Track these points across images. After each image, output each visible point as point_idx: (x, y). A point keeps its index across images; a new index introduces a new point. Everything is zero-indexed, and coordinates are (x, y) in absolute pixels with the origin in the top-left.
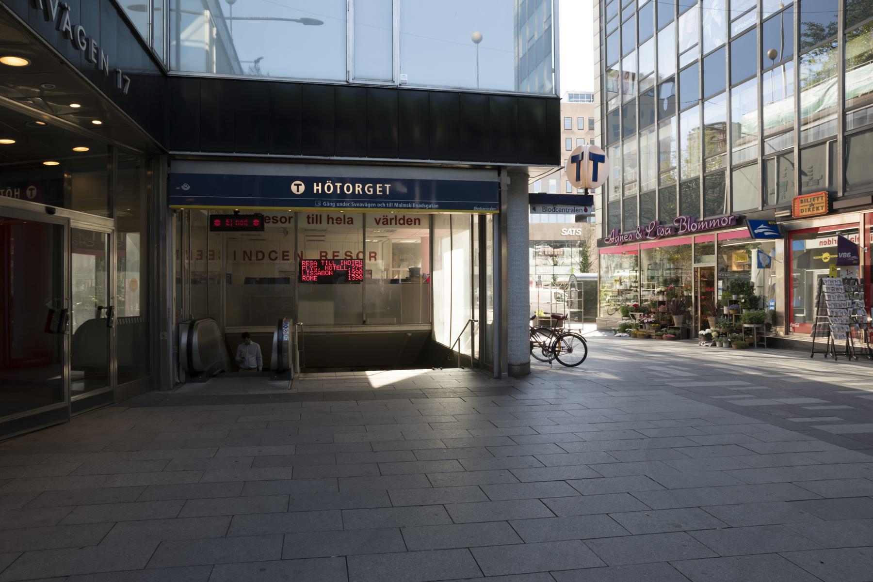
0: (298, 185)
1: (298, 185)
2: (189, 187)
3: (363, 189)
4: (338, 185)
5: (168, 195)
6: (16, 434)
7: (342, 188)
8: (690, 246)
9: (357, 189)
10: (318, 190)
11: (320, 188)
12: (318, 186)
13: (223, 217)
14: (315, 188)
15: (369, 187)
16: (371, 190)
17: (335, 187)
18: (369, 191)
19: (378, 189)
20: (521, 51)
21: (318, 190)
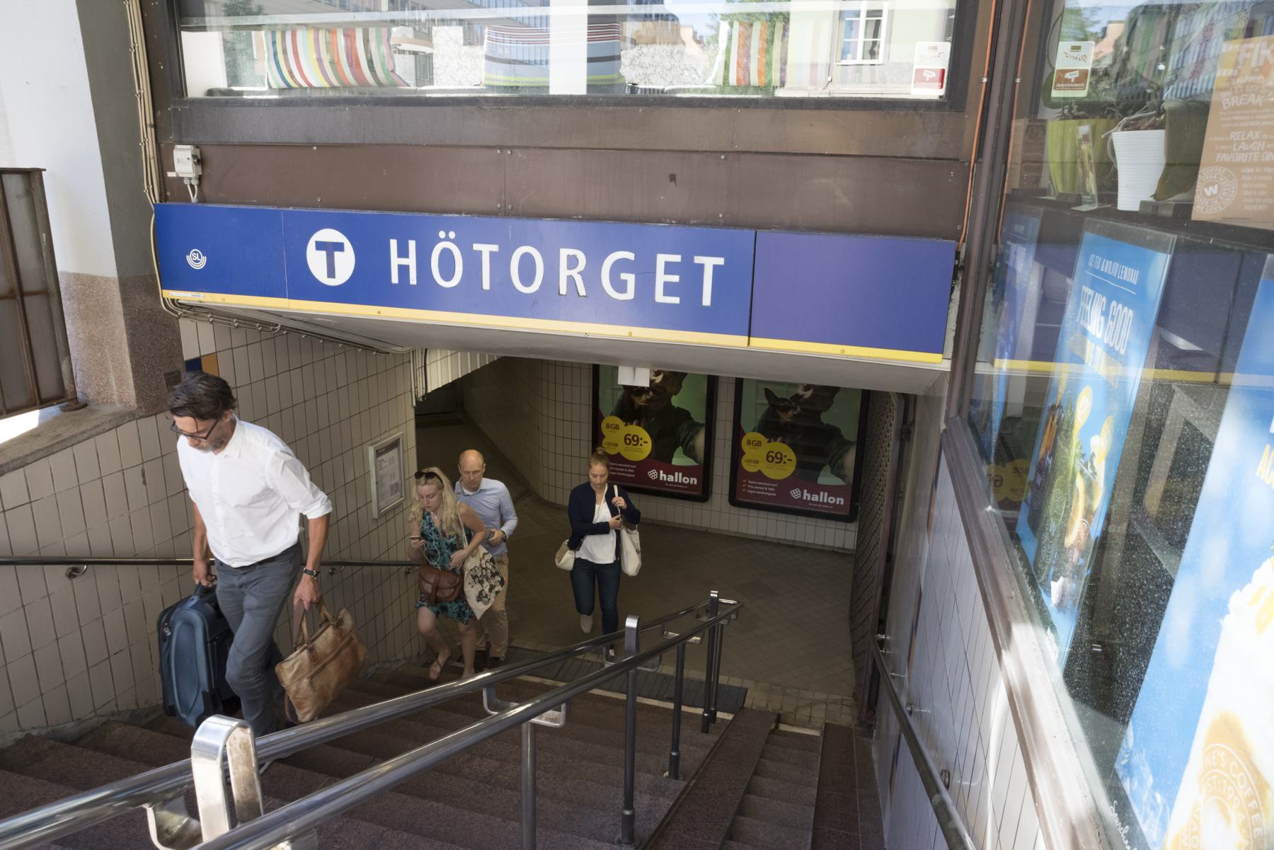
3: (591, 276)
7: (501, 262)
11: (411, 261)
12: (403, 252)
14: (395, 261)
16: (630, 278)
17: (473, 261)
18: (620, 286)
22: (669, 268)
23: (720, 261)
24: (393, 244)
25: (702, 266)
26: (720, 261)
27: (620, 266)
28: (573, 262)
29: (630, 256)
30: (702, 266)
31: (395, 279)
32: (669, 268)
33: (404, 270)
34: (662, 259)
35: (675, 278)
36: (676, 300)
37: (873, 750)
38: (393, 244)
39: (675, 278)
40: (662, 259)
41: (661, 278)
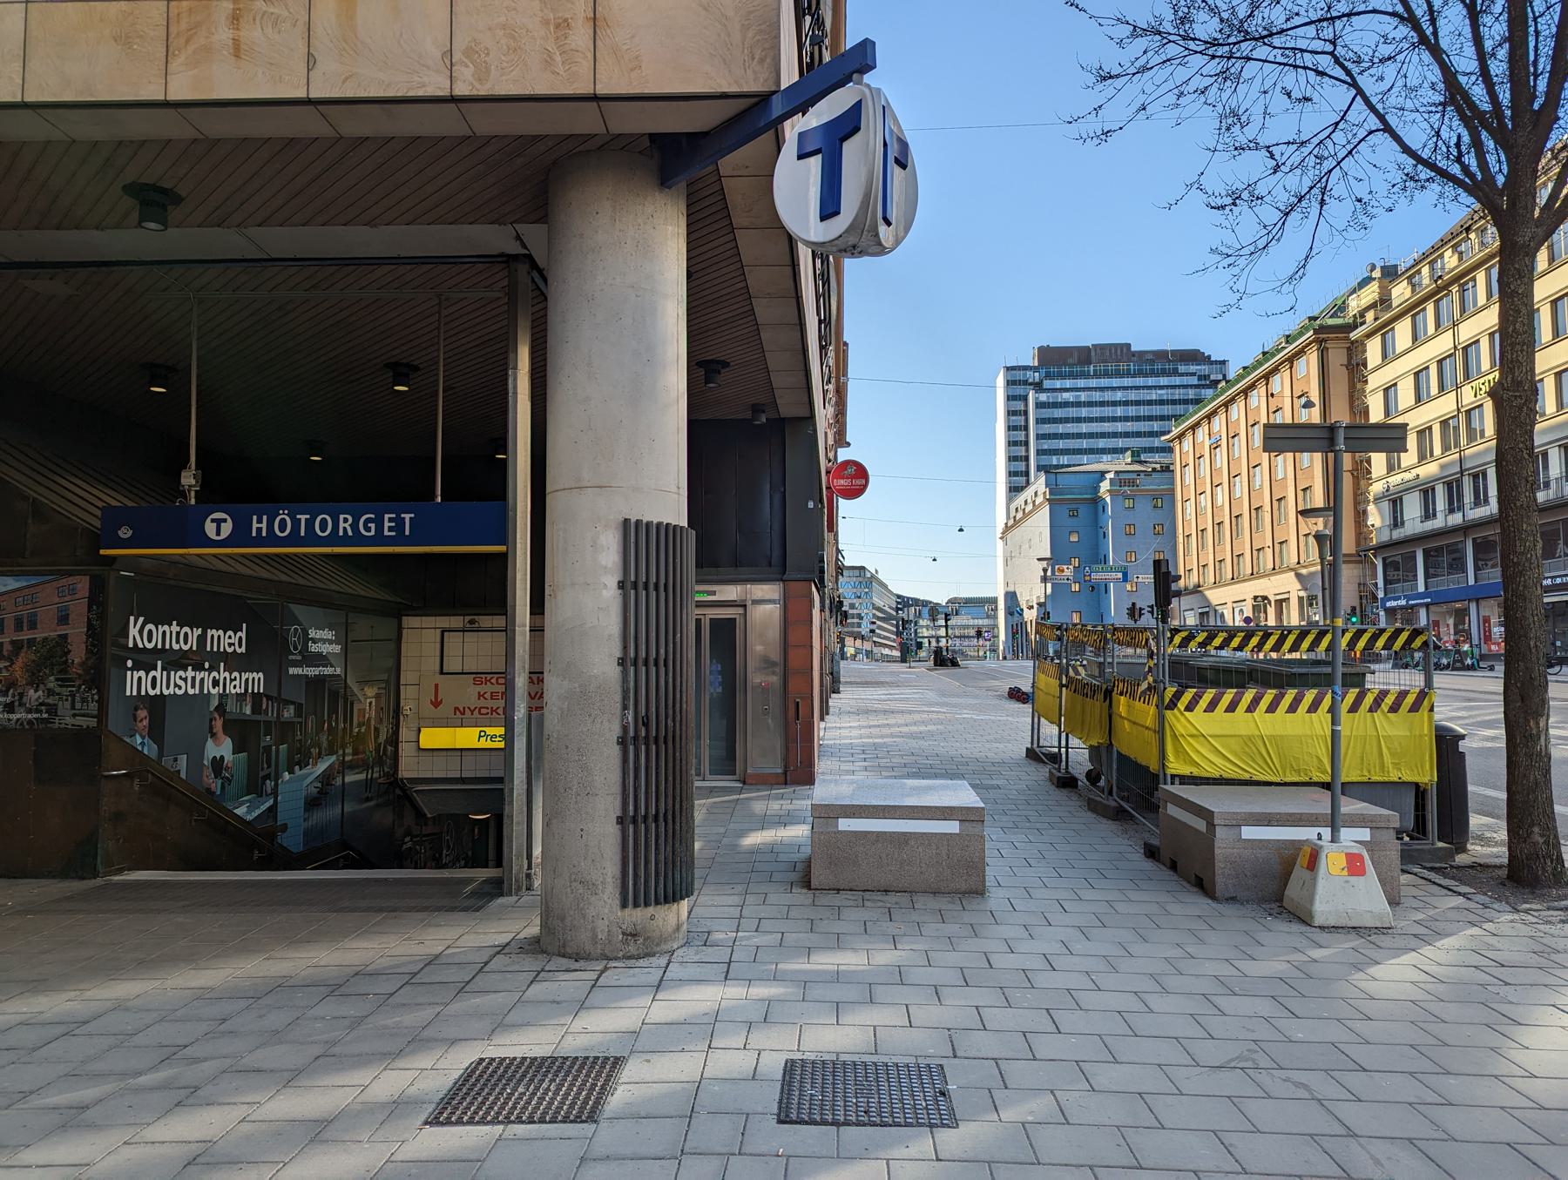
0: (219, 522)
1: (219, 522)
2: (130, 532)
3: (355, 526)
4: (303, 518)
5: (499, 819)
6: (1532, 45)
7: (310, 524)
8: (994, 601)
9: (342, 525)
10: (259, 530)
11: (264, 525)
13: (830, 1071)
14: (255, 525)
15: (367, 521)
16: (372, 526)
18: (368, 530)
19: (387, 524)
20: (1456, 297)
21: (259, 530)
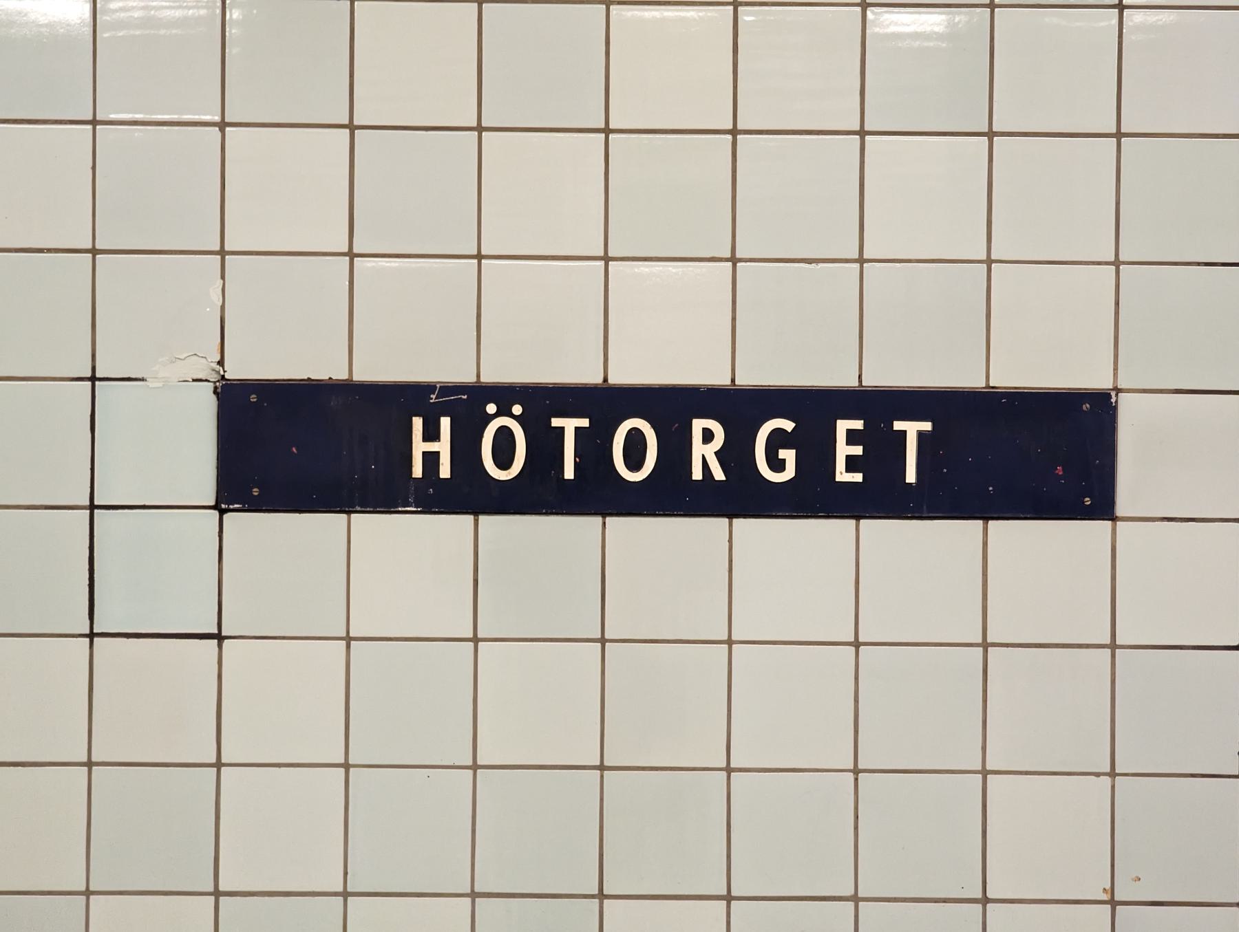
11: (443, 447)
14: (419, 447)
18: (778, 465)
22: (852, 437)
23: (927, 426)
24: (445, 472)
25: (903, 433)
26: (927, 426)
27: (777, 440)
28: (708, 436)
29: (788, 426)
30: (903, 433)
31: (417, 471)
32: (852, 437)
33: (431, 460)
34: (843, 426)
35: (858, 450)
36: (858, 477)
37: (932, 21)
38: (445, 472)
39: (858, 450)
40: (843, 426)
41: (844, 450)
